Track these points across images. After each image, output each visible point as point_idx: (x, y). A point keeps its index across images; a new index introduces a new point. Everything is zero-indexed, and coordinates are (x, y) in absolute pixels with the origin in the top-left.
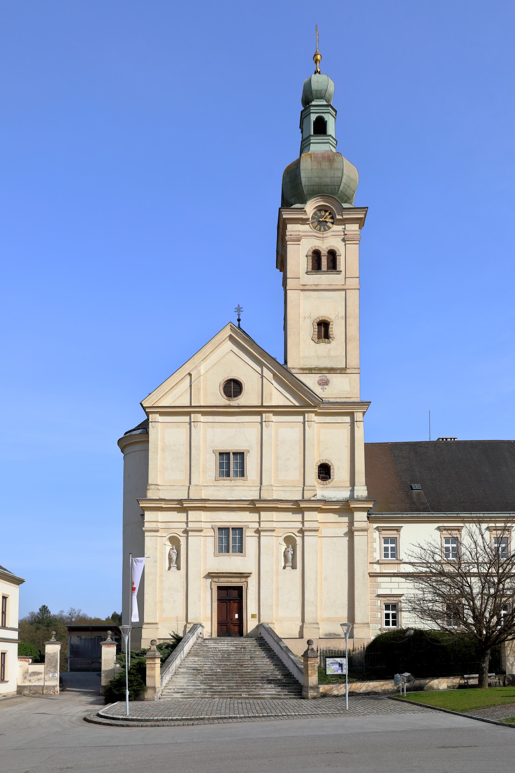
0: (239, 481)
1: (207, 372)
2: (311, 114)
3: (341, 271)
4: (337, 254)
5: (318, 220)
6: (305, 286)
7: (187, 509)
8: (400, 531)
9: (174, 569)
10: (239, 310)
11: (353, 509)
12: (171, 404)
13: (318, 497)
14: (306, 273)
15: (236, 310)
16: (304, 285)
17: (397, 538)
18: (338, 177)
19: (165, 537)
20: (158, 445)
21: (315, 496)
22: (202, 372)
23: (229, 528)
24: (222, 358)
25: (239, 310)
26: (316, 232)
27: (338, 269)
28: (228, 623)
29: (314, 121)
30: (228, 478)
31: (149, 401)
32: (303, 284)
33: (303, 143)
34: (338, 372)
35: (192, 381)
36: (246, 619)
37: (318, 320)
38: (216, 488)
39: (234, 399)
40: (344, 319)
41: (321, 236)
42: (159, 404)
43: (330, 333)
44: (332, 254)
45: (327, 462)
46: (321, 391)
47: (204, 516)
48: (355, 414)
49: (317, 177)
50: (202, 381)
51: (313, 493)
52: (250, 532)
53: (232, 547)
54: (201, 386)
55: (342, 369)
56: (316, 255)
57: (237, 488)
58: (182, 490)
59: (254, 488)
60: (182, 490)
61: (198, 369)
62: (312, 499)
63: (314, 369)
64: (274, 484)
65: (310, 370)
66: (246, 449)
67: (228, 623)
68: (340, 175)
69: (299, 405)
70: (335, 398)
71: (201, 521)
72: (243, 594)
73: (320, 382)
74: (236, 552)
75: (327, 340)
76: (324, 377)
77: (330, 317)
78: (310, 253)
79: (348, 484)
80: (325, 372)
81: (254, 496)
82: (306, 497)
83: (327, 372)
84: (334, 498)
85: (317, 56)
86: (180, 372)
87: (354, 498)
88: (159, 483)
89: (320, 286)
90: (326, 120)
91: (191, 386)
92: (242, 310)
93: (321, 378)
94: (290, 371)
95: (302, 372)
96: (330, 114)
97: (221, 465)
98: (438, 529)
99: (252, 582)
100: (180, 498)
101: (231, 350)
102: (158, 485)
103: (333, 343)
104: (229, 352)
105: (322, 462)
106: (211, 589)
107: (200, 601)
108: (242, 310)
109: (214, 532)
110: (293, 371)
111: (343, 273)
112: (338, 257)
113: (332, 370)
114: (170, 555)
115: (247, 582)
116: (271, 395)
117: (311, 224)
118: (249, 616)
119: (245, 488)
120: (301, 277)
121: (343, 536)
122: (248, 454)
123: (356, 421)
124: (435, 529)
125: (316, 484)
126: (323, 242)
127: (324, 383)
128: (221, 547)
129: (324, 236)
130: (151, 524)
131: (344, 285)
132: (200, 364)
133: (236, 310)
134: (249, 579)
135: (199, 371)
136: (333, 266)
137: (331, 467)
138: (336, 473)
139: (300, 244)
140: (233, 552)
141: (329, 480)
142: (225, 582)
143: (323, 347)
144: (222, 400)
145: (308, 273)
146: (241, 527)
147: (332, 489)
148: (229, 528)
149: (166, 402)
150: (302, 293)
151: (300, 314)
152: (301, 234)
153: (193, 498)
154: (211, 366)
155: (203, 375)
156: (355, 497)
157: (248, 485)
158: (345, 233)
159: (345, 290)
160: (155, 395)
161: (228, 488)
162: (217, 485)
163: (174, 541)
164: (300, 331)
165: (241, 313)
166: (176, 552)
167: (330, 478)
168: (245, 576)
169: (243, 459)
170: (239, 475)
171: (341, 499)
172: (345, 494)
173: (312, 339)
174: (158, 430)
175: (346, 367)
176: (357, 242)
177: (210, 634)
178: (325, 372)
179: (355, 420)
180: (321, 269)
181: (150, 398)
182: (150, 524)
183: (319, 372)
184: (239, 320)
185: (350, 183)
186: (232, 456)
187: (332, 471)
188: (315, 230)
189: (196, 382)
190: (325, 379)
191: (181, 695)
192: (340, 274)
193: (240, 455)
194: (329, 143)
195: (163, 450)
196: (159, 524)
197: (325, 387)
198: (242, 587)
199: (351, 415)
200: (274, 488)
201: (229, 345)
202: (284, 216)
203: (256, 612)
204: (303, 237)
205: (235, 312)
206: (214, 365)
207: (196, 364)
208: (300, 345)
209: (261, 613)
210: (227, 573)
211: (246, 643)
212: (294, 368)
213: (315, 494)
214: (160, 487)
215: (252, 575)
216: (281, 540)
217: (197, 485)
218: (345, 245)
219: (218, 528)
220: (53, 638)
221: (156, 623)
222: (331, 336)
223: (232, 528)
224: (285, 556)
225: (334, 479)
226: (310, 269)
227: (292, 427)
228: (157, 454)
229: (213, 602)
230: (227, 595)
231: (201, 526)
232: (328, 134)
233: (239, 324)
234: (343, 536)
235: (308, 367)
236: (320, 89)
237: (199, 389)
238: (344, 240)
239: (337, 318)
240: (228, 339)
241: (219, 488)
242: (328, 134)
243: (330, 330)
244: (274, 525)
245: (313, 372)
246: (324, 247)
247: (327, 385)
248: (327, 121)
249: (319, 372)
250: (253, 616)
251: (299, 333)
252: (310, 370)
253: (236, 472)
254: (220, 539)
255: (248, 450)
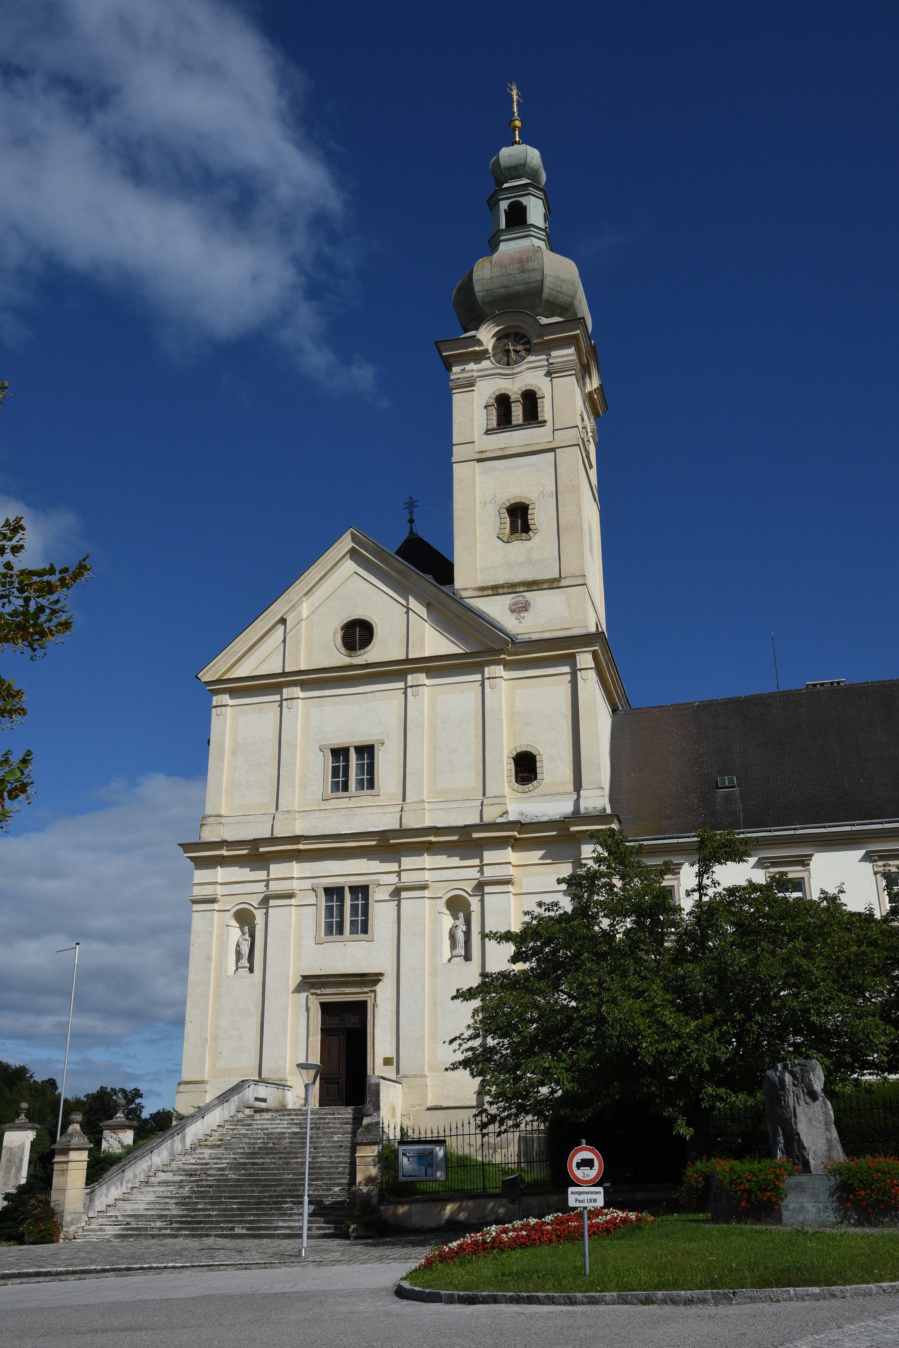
0: (366, 799)
1: (313, 612)
2: (501, 202)
3: (545, 421)
4: (537, 396)
5: (503, 349)
6: (484, 453)
7: (480, 842)
8: (809, 865)
9: (244, 972)
10: (411, 505)
11: (577, 835)
12: (250, 673)
13: (512, 817)
14: (487, 431)
15: (406, 506)
16: (482, 452)
17: (804, 878)
18: (538, 281)
19: (229, 910)
20: (224, 744)
21: (505, 816)
22: (305, 614)
23: (343, 888)
24: (339, 587)
25: (411, 505)
26: (502, 368)
27: (540, 419)
28: (340, 1078)
29: (505, 210)
30: (345, 794)
31: (211, 672)
32: (481, 450)
33: (492, 243)
34: (545, 586)
35: (287, 632)
36: (372, 1067)
37: (508, 504)
38: (322, 814)
39: (362, 652)
40: (555, 497)
41: (510, 372)
42: (231, 675)
43: (530, 522)
44: (530, 398)
45: (528, 749)
46: (516, 622)
47: (296, 869)
48: (578, 657)
49: (502, 288)
50: (303, 629)
51: (499, 810)
52: (383, 893)
53: (351, 923)
54: (301, 637)
55: (554, 580)
56: (503, 402)
57: (359, 811)
58: (262, 822)
59: (391, 809)
60: (262, 822)
61: (298, 609)
62: (499, 820)
63: (502, 586)
64: (429, 799)
65: (495, 590)
66: (378, 738)
67: (340, 1078)
68: (539, 278)
69: (454, 649)
70: (542, 632)
71: (292, 878)
72: (368, 1017)
73: (514, 607)
74: (357, 933)
75: (524, 535)
76: (520, 599)
77: (530, 496)
78: (492, 401)
79: (570, 788)
80: (521, 589)
81: (390, 823)
82: (487, 819)
83: (525, 589)
84: (544, 816)
85: (513, 122)
86: (265, 618)
87: (580, 813)
88: (223, 812)
89: (509, 449)
90: (524, 205)
91: (284, 641)
92: (415, 504)
93: (515, 600)
94: (459, 594)
95: (480, 593)
96: (531, 196)
97: (335, 772)
98: (868, 858)
99: (384, 991)
100: (251, 837)
101: (356, 573)
102: (220, 816)
103: (536, 539)
104: (352, 575)
105: (519, 751)
106: (308, 1009)
107: (285, 1033)
108: (415, 504)
109: (316, 896)
110: (464, 594)
111: (549, 423)
112: (539, 401)
113: (533, 585)
114: (238, 945)
115: (374, 991)
116: (423, 639)
117: (492, 358)
118: (379, 1061)
119: (374, 810)
120: (476, 439)
121: (388, 898)
122: (381, 748)
123: (580, 670)
124: (860, 861)
125: (507, 790)
126: (513, 382)
127: (521, 609)
128: (329, 925)
129: (515, 371)
130: (205, 888)
131: (551, 442)
132: (300, 602)
133: (406, 506)
134: (379, 988)
135: (300, 614)
136: (532, 416)
137: (538, 758)
138: (545, 768)
139: (473, 390)
140: (351, 933)
141: (535, 783)
142: (335, 996)
143: (519, 547)
144: (337, 657)
145: (488, 433)
146: (365, 884)
147: (539, 799)
148: (343, 888)
149: (242, 671)
150: (478, 466)
151: (475, 498)
152: (475, 374)
153: (280, 836)
154: (321, 601)
155: (307, 618)
156: (582, 810)
157: (379, 804)
158: (550, 362)
159: (553, 450)
160: (221, 661)
161: (343, 812)
162: (325, 808)
163: (244, 918)
164: (475, 526)
165: (414, 509)
166: (249, 939)
167: (536, 778)
168: (371, 980)
169: (372, 757)
170: (342, 788)
171: (558, 817)
172: (565, 807)
173: (498, 537)
174: (225, 721)
175: (560, 577)
176: (573, 372)
177: (303, 1102)
178: (521, 589)
179: (578, 667)
180: (511, 423)
181: (212, 667)
182: (203, 888)
183: (510, 590)
184: (411, 521)
185: (561, 287)
186: (353, 755)
187: (538, 765)
188: (498, 365)
189: (293, 631)
190: (522, 602)
191: (119, 1230)
192: (544, 426)
193: (367, 751)
194: (530, 236)
195: (234, 753)
196: (218, 886)
197: (522, 615)
198: (366, 1002)
199: (571, 660)
200: (427, 806)
201: (350, 566)
202: (572, 350)
203: (391, 1053)
204: (478, 379)
205: (404, 509)
206: (326, 599)
207: (293, 602)
208: (476, 548)
209: (401, 1054)
210: (334, 976)
211: (328, 1118)
212: (466, 589)
213: (504, 811)
214: (224, 820)
215: (384, 978)
216: (441, 905)
217: (289, 812)
218: (551, 380)
219: (324, 888)
220: (23, 1116)
221: (203, 1082)
222: (532, 527)
223: (350, 888)
224: (452, 937)
225: (544, 781)
226: (494, 423)
227: (462, 692)
228: (223, 761)
229: (311, 1035)
230: (340, 1020)
231: (292, 886)
232: (528, 223)
233: (411, 528)
234: (388, 898)
235: (492, 583)
236: (515, 165)
237: (298, 643)
238: (549, 374)
239: (541, 496)
240: (348, 556)
241: (327, 814)
242: (528, 223)
243: (529, 517)
244: (427, 876)
245: (501, 591)
246: (514, 387)
247: (526, 610)
248: (526, 206)
249: (510, 590)
250: (387, 1062)
251: (474, 530)
252: (495, 590)
253: (360, 784)
254: (329, 909)
255: (381, 740)
